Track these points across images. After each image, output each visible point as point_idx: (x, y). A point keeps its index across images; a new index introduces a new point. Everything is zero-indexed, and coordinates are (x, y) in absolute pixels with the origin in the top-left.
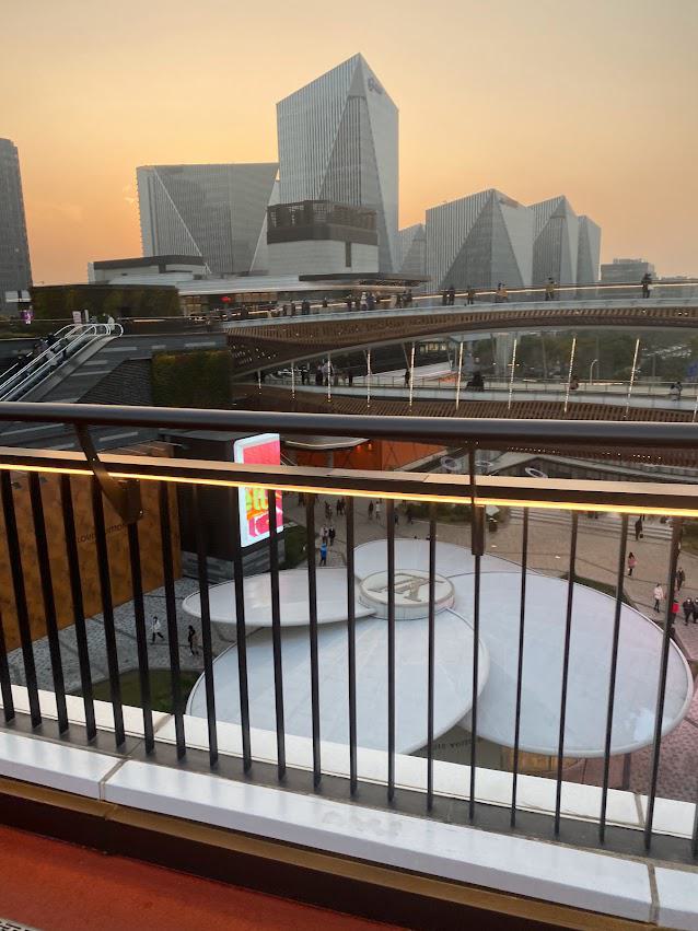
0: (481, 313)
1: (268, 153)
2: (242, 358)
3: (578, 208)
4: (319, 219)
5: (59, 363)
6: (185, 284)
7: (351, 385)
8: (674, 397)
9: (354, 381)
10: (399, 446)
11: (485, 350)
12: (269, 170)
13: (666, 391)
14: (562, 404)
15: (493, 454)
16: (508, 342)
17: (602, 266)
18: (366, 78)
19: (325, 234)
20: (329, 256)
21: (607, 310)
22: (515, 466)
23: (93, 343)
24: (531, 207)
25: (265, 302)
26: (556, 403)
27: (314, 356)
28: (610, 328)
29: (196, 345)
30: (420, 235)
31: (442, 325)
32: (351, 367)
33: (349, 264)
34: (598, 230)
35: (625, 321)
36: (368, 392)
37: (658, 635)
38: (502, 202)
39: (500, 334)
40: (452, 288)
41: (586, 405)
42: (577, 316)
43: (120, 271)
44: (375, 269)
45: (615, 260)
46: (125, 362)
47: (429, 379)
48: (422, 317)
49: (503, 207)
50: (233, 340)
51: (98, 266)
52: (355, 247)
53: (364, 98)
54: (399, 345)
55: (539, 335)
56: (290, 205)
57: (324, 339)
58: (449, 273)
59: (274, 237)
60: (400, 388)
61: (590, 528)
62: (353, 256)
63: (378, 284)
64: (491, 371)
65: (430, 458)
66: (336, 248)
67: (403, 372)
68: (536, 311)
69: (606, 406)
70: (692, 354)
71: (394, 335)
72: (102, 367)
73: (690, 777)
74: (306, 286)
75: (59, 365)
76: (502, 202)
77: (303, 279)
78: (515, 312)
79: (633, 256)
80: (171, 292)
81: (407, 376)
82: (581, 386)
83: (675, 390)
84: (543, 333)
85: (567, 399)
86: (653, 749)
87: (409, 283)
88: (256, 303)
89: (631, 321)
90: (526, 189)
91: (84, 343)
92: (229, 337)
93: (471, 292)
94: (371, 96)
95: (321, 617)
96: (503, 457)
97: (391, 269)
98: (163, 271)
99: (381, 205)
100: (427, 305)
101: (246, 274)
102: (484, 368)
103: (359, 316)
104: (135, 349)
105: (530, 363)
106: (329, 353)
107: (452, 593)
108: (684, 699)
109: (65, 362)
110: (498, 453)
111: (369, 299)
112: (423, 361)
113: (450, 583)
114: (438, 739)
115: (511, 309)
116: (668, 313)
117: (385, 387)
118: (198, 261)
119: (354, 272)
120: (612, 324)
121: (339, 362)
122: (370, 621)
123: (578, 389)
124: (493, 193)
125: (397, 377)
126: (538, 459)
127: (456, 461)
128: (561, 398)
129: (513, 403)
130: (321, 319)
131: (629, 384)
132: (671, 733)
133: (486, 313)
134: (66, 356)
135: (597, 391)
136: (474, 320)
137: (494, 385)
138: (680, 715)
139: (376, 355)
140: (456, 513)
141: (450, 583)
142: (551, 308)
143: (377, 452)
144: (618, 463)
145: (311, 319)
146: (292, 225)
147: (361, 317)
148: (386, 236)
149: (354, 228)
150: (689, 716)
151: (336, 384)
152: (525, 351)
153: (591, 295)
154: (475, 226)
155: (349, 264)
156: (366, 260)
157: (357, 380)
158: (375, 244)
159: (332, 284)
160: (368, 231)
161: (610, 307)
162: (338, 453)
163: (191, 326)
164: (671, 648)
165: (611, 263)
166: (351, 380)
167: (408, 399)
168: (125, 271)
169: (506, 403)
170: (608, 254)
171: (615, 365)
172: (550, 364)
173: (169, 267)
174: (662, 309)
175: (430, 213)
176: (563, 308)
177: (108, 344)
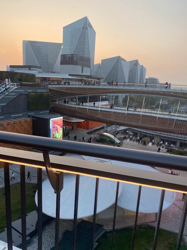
0: (120, 89)
1: (60, 40)
2: (52, 96)
3: (141, 63)
4: (75, 59)
5: (4, 91)
6: (39, 74)
7: (82, 105)
12: (59, 45)
13: (167, 113)
14: (140, 115)
15: (118, 126)
16: (121, 96)
18: (88, 23)
19: (76, 64)
20: (77, 70)
22: (123, 130)
23: (12, 88)
24: (129, 62)
25: (59, 81)
27: (72, 97)
29: (41, 91)
31: (109, 91)
32: (83, 100)
33: (82, 72)
34: (146, 69)
35: (158, 94)
36: (88, 108)
38: (121, 59)
39: (120, 95)
40: (112, 81)
43: (17, 68)
44: (89, 74)
45: (149, 78)
46: (20, 94)
47: (101, 105)
50: (51, 90)
51: (11, 66)
52: (85, 68)
53: (87, 28)
54: (97, 96)
56: (67, 55)
57: (77, 92)
59: (62, 63)
60: (92, 107)
61: (144, 148)
62: (84, 70)
63: (90, 78)
64: (117, 104)
65: (101, 126)
66: (79, 68)
69: (133, 114)
72: (14, 95)
73: (173, 218)
74: (70, 77)
75: (4, 92)
76: (121, 59)
77: (69, 75)
79: (154, 77)
80: (33, 76)
81: (94, 104)
82: (137, 110)
85: (126, 112)
87: (98, 79)
88: (56, 81)
89: (158, 94)
90: (128, 57)
91: (9, 88)
92: (50, 89)
93: (117, 83)
94: (89, 28)
98: (29, 69)
100: (104, 85)
101: (54, 72)
103: (87, 87)
104: (23, 91)
106: (77, 97)
109: (6, 91)
110: (119, 126)
112: (103, 100)
113: (111, 162)
116: (165, 92)
118: (40, 68)
119: (84, 74)
120: (156, 95)
124: (119, 57)
125: (92, 104)
127: (109, 128)
128: (140, 113)
129: (127, 114)
131: (158, 111)
134: (6, 89)
136: (118, 90)
137: (117, 108)
140: (109, 142)
143: (88, 123)
146: (67, 60)
147: (87, 87)
150: (174, 203)
151: (79, 105)
152: (125, 100)
153: (142, 86)
155: (82, 72)
156: (87, 72)
157: (84, 104)
159: (77, 77)
163: (38, 85)
165: (148, 78)
166: (82, 104)
168: (19, 69)
170: (148, 75)
171: (151, 104)
172: (132, 103)
173: (31, 69)
176: (142, 89)
177: (16, 89)
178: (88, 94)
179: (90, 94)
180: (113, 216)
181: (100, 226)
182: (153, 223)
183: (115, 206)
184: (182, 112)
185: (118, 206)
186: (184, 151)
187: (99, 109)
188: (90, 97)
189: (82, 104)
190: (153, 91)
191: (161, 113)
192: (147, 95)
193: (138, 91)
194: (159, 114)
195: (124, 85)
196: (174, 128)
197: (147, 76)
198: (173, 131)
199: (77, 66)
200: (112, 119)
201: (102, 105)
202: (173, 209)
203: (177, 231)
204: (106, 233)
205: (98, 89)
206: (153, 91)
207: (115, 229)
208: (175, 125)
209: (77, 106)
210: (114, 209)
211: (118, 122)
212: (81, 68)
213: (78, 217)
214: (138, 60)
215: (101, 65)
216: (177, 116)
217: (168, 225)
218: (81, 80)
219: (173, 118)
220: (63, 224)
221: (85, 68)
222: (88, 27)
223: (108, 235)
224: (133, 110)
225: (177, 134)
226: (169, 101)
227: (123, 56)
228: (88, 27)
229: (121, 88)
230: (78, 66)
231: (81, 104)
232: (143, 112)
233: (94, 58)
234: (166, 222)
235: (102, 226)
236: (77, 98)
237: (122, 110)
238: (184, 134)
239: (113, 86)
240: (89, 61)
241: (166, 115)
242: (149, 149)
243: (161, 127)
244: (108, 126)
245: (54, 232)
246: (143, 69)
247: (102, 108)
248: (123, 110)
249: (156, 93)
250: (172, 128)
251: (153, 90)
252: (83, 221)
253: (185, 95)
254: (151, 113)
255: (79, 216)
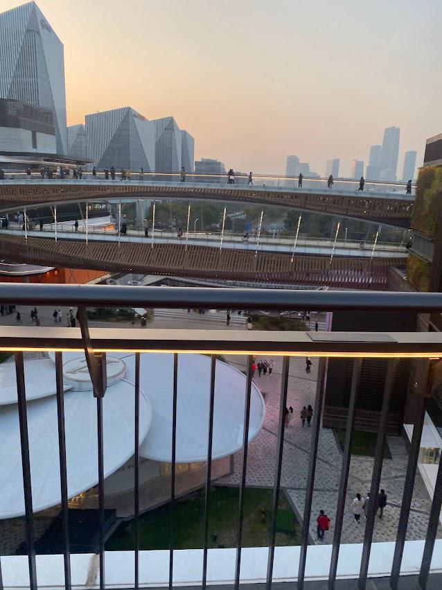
0: (132, 186)
3: (181, 125)
7: (41, 230)
8: (246, 243)
9: (44, 227)
10: (76, 271)
11: (130, 210)
13: (240, 239)
14: (184, 246)
15: (140, 276)
17: (196, 162)
18: (39, 19)
19: (15, 124)
21: (208, 190)
26: (181, 245)
28: (203, 200)
30: (81, 132)
32: (42, 216)
36: (56, 235)
37: (244, 379)
38: (135, 116)
41: (198, 247)
42: (191, 192)
44: (54, 152)
45: (203, 159)
47: (95, 228)
48: (93, 186)
49: (136, 120)
52: (39, 136)
53: (38, 33)
55: (161, 202)
57: (21, 197)
58: (102, 159)
63: (58, 161)
64: (134, 223)
66: (25, 135)
67: (74, 222)
68: (166, 188)
70: (247, 218)
71: (73, 197)
78: (154, 187)
79: (213, 158)
81: (76, 225)
83: (246, 239)
84: (164, 201)
86: (243, 452)
87: (78, 163)
89: (222, 197)
90: (150, 109)
94: (43, 32)
95: (30, 394)
96: (146, 277)
97: (63, 152)
99: (54, 108)
102: (130, 221)
103: (47, 182)
105: (161, 218)
106: (25, 208)
107: (124, 369)
108: (262, 416)
110: (142, 275)
111: (61, 172)
112: (94, 214)
113: (123, 362)
114: (109, 477)
115: (151, 185)
117: (68, 232)
121: (31, 214)
122: (70, 393)
123: (183, 236)
125: (69, 225)
126: (167, 279)
129: (155, 245)
130: (65, 183)
131: (220, 234)
132: (253, 441)
133: (135, 186)
135: (193, 238)
136: (127, 190)
138: (260, 426)
139: (60, 210)
140: (120, 315)
141: (123, 362)
142: (217, 188)
144: (216, 281)
145: (82, 182)
148: (58, 130)
149: (37, 122)
151: (31, 229)
154: (119, 129)
155: (35, 146)
156: (47, 145)
157: (46, 226)
158: (54, 135)
160: (48, 125)
161: (210, 188)
162: (31, 277)
164: (252, 387)
165: (201, 160)
166: (41, 227)
167: (85, 241)
169: (150, 244)
171: (209, 221)
174: (238, 191)
175: (88, 118)
178: (56, 201)
179: (58, 201)
180: (133, 486)
181: (111, 512)
182: (224, 479)
183: (136, 462)
184: (276, 234)
185: (140, 458)
186: (282, 316)
187: (87, 237)
188: (60, 210)
189: (41, 227)
190: (206, 191)
191: (228, 238)
192: (197, 200)
193: (223, 192)
194: (224, 241)
195: (141, 178)
196: (255, 269)
197: (198, 156)
198: (253, 275)
199: (18, 129)
200: (122, 261)
201: (94, 227)
202: (265, 440)
203: (272, 484)
204: (124, 524)
205: (79, 187)
206: (205, 190)
207: (140, 514)
208: (258, 263)
209: (26, 234)
210: (133, 470)
211: (139, 267)
212: (31, 136)
213: (33, 508)
214: (175, 118)
215: (84, 128)
216: (260, 243)
217: (256, 475)
218: (35, 167)
219: (251, 247)
220: (11, 532)
221: (40, 137)
222: (40, 28)
223: (128, 529)
224: (176, 235)
225: (266, 281)
226: (247, 212)
227: (138, 108)
228: (40, 28)
229: (134, 183)
230: (22, 130)
231: (38, 227)
232: (189, 239)
233: (64, 111)
234: (252, 471)
235: (114, 511)
236: (25, 211)
237: (350, 249)
238: (273, 280)
239: (127, 180)
240: (49, 116)
241: (238, 242)
242: (210, 321)
243: (229, 270)
244: (115, 278)
245: (427, 519)
246: (186, 140)
247: (92, 233)
248: (157, 237)
249: (203, 194)
250: (252, 270)
251: (206, 187)
252: (43, 515)
253: (279, 196)
254: (208, 240)
255: (37, 507)
